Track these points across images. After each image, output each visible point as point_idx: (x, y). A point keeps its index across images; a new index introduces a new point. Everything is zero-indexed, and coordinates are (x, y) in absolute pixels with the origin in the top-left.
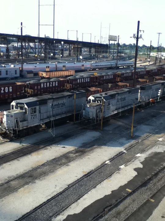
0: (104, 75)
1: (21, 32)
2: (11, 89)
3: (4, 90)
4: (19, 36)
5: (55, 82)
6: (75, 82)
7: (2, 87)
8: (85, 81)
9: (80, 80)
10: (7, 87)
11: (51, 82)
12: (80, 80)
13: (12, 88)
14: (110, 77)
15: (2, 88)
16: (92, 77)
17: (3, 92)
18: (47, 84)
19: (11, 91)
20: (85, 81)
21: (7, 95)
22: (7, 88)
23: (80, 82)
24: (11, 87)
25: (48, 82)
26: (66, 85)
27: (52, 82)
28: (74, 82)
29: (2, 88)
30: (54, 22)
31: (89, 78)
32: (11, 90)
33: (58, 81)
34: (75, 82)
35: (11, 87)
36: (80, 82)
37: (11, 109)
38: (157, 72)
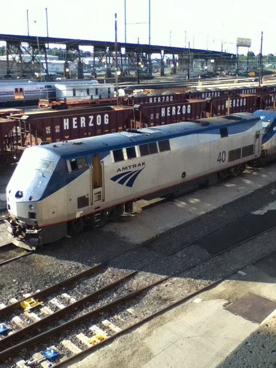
0: (213, 90)
1: (117, 36)
2: (108, 119)
3: (94, 121)
4: (113, 43)
5: (169, 96)
6: (155, 116)
7: (91, 115)
8: (179, 113)
9: (168, 111)
10: (99, 114)
11: (164, 96)
12: (168, 111)
13: (109, 118)
14: (239, 103)
15: (90, 117)
16: (177, 95)
17: (92, 125)
18: (157, 100)
19: (108, 123)
20: (179, 113)
21: (100, 130)
22: (84, 118)
23: (169, 115)
24: (107, 115)
25: (159, 96)
26: (133, 123)
27: (165, 96)
28: (152, 115)
29: (90, 117)
30: (116, 29)
31: (219, 93)
32: (106, 122)
33: (173, 95)
34: (155, 116)
35: (107, 115)
36: (169, 115)
37: (240, 158)
38: (122, 238)
